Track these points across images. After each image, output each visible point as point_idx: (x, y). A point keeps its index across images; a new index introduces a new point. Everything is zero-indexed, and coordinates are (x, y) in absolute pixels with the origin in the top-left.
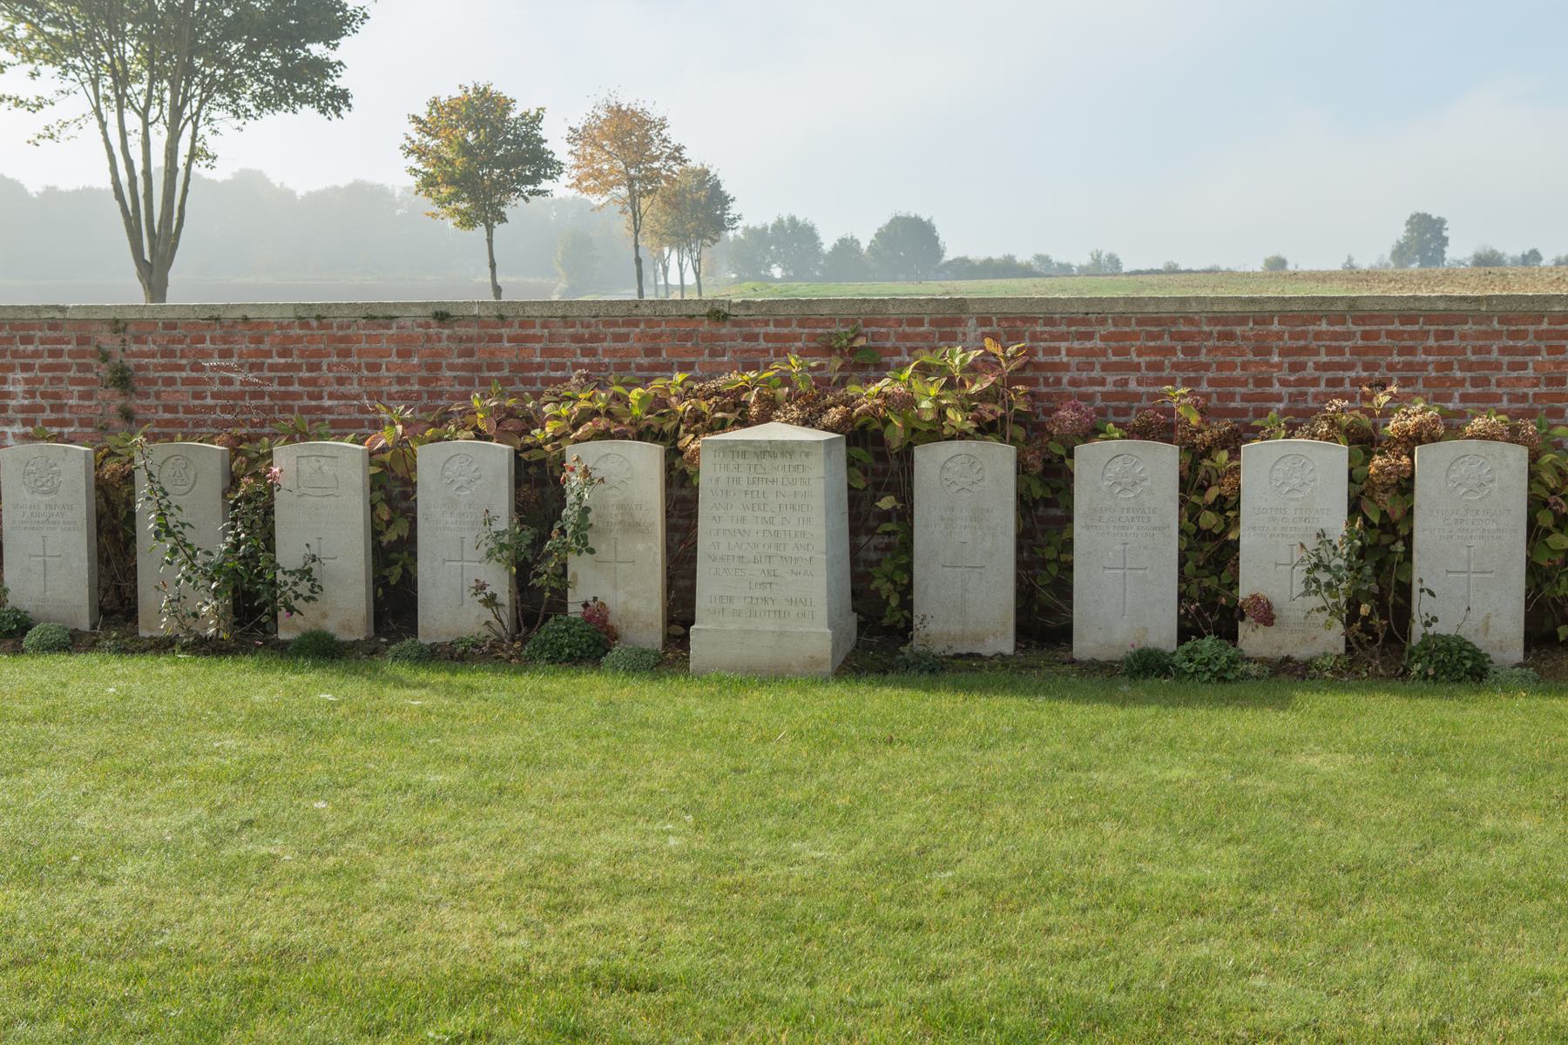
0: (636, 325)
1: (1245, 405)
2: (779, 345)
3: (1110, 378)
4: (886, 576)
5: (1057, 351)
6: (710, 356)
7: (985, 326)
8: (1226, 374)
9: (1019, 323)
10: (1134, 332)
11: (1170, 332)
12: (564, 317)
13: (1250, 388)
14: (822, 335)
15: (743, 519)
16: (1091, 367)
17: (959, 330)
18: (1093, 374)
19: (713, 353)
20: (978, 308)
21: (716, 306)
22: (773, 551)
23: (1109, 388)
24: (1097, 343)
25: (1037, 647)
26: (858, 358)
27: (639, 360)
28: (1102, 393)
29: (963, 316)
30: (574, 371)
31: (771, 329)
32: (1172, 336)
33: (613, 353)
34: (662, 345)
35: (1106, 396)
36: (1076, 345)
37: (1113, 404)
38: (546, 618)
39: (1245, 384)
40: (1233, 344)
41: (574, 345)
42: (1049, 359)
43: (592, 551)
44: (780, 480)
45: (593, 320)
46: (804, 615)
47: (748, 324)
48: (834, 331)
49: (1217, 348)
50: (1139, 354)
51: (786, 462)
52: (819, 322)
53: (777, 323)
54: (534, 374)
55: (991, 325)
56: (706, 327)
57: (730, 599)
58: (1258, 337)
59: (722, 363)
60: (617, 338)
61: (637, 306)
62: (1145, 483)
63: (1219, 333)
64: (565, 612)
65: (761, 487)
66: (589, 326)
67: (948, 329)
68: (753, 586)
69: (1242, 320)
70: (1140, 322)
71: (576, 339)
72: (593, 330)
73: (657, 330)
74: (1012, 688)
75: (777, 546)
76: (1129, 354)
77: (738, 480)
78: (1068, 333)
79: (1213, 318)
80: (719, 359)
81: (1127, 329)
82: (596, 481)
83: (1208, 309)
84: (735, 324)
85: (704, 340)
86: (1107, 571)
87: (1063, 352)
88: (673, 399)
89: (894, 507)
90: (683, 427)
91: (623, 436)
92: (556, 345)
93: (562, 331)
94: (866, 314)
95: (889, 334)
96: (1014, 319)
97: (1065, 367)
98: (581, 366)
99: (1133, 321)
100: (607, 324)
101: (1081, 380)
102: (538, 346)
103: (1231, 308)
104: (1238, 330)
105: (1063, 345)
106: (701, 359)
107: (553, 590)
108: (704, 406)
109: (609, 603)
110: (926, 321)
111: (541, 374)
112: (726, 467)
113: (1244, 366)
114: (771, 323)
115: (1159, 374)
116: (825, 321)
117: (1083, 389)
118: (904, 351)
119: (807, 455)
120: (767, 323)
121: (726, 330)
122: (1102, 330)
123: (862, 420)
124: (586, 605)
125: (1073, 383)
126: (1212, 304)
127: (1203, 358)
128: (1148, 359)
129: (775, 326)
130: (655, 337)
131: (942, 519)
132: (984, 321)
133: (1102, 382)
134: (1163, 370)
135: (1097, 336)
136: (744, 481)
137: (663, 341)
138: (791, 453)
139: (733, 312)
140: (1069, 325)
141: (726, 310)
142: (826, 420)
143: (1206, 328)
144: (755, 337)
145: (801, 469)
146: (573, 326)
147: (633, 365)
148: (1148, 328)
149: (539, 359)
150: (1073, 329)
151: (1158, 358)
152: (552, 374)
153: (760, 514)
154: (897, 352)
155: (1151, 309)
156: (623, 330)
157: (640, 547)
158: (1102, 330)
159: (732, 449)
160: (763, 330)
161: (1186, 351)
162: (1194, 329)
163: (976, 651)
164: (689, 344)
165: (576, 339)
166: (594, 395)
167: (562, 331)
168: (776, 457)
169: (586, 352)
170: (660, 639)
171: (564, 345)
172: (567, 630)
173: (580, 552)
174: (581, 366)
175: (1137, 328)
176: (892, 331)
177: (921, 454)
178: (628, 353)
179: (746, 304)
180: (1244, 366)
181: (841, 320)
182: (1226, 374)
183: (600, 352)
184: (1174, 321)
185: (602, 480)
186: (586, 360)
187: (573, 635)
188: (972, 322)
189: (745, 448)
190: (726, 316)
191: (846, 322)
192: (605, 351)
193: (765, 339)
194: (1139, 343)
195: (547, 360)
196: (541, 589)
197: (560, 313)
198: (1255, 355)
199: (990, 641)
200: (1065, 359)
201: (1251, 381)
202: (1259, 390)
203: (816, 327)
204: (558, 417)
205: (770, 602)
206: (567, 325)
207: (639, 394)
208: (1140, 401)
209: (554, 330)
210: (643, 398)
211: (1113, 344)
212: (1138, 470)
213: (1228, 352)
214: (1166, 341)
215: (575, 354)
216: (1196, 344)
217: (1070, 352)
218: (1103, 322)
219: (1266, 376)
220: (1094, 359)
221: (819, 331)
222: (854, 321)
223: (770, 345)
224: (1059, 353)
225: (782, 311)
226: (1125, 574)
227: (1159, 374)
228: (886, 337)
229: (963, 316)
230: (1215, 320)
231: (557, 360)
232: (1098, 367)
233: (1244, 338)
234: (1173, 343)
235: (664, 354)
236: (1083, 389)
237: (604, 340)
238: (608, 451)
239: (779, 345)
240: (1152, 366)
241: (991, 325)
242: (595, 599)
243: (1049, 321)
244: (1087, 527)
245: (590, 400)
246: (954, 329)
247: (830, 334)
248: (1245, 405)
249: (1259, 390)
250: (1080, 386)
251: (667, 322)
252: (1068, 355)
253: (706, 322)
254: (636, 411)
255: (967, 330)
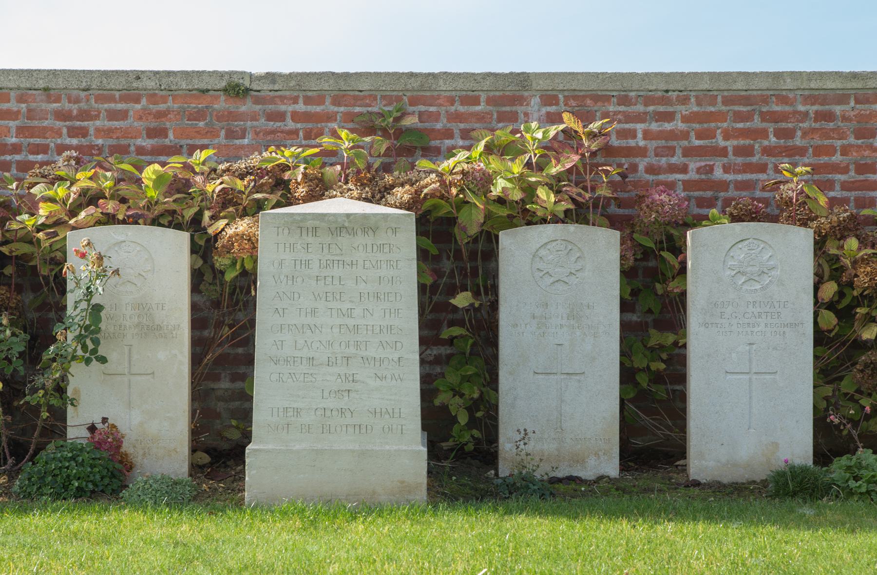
0: (137, 100)
1: (846, 194)
2: (310, 125)
3: (694, 164)
4: (452, 390)
5: (633, 134)
6: (227, 137)
7: (551, 105)
8: (824, 159)
9: (589, 102)
10: (720, 112)
11: (762, 114)
12: (46, 89)
13: (852, 175)
14: (361, 114)
15: (314, 312)
16: (671, 151)
17: (520, 109)
18: (674, 160)
19: (231, 134)
20: (543, 85)
21: (236, 80)
22: (352, 350)
23: (692, 175)
24: (678, 125)
25: (168, 505)
26: (405, 141)
27: (139, 142)
28: (684, 182)
29: (526, 94)
30: (59, 154)
31: (301, 107)
32: (764, 117)
33: (108, 133)
34: (168, 125)
35: (688, 185)
36: (654, 126)
37: (697, 194)
38: (40, 448)
39: (845, 170)
40: (831, 125)
41: (58, 124)
42: (623, 143)
43: (103, 360)
44: (361, 262)
45: (83, 94)
46: (391, 429)
47: (272, 101)
48: (375, 109)
49: (813, 130)
50: (726, 137)
51: (368, 240)
52: (357, 99)
53: (308, 101)
54: (8, 158)
55: (557, 104)
56: (222, 104)
57: (298, 411)
58: (860, 118)
59: (242, 147)
60: (113, 115)
61: (138, 78)
62: (773, 273)
63: (816, 112)
64: (63, 434)
65: (337, 271)
66: (77, 101)
67: (508, 109)
68: (326, 394)
69: (842, 99)
70: (727, 101)
71: (62, 116)
72: (83, 105)
73: (162, 107)
74: (612, 513)
75: (357, 345)
76: (714, 137)
77: (308, 263)
78: (645, 113)
79: (810, 96)
80: (238, 142)
81: (713, 109)
82: (109, 274)
83: (805, 86)
84: (258, 101)
85: (219, 119)
86: (729, 377)
87: (640, 135)
88: (198, 179)
89: (472, 305)
90: (207, 214)
91: (134, 220)
92: (36, 123)
93: (44, 106)
94: (413, 90)
95: (439, 114)
96: (585, 97)
97: (642, 152)
98: (69, 148)
99: (719, 99)
100: (100, 99)
101: (660, 167)
102: (13, 124)
103: (830, 85)
104: (838, 109)
105: (640, 127)
106: (216, 141)
107: (50, 408)
108: (240, 185)
109: (123, 428)
110: (483, 98)
111: (18, 157)
112: (292, 247)
113: (845, 151)
114: (301, 101)
115: (749, 159)
116: (365, 97)
117: (662, 177)
118: (457, 132)
119: (395, 231)
120: (295, 100)
121: (246, 107)
122: (683, 110)
123: (428, 204)
124: (92, 428)
125: (651, 170)
126: (810, 80)
127: (798, 141)
128: (735, 143)
129: (305, 104)
130: (160, 115)
131: (534, 317)
132: (549, 99)
133: (684, 169)
134: (753, 155)
135: (678, 116)
136: (315, 265)
137: (170, 120)
138: (374, 230)
139: (255, 87)
140: (646, 105)
141: (247, 83)
142: (390, 199)
143: (801, 108)
144: (280, 116)
145: (387, 250)
146: (58, 100)
147: (132, 148)
148: (737, 108)
149: (14, 140)
150: (651, 108)
151: (748, 142)
152: (31, 158)
153: (334, 305)
154: (448, 134)
155: (739, 85)
156: (120, 106)
157: (162, 355)
158: (683, 110)
159: (301, 224)
160: (291, 108)
161: (778, 134)
162: (787, 108)
163: (575, 474)
164: (201, 124)
165: (62, 116)
166: (95, 174)
167: (44, 106)
168: (355, 234)
169: (73, 132)
170: (185, 468)
171: (46, 123)
172: (73, 458)
173: (88, 361)
174: (69, 148)
175: (724, 108)
176: (443, 110)
177: (507, 240)
178: (127, 133)
179: (271, 77)
180: (845, 151)
181: (383, 97)
182: (824, 159)
183: (92, 131)
184: (765, 100)
185: (116, 272)
186: (75, 141)
187: (82, 464)
188: (535, 101)
189: (317, 223)
190: (247, 90)
191: (389, 99)
192: (98, 130)
193: (293, 120)
194: (725, 125)
195: (25, 141)
196: (35, 410)
197: (41, 84)
198: (857, 138)
199: (592, 462)
200: (642, 143)
201: (852, 167)
202: (862, 177)
203: (354, 105)
204: (52, 200)
205: (348, 414)
206: (49, 99)
207: (155, 172)
208: (727, 190)
209: (33, 105)
210: (159, 179)
211: (697, 126)
212: (766, 257)
213: (826, 135)
214: (757, 123)
215: (60, 135)
216: (790, 125)
217: (647, 135)
218: (685, 100)
219: (869, 161)
220: (674, 143)
221: (357, 109)
222: (399, 99)
223: (299, 126)
224: (634, 136)
225: (314, 85)
226: (750, 379)
227: (749, 159)
228: (436, 117)
229: (526, 94)
230: (811, 99)
231: (38, 141)
232: (679, 152)
233: (844, 118)
234: (764, 125)
235: (171, 135)
236: (662, 177)
237: (97, 117)
238: (121, 238)
239: (310, 125)
240: (740, 151)
241: (557, 104)
242: (105, 420)
243: (624, 100)
244: (706, 325)
245: (91, 178)
246: (514, 108)
247: (370, 113)
248: (846, 194)
249: (862, 177)
250: (658, 174)
251: (175, 98)
252: (645, 138)
253: (223, 98)
254: (152, 193)
255: (529, 109)
